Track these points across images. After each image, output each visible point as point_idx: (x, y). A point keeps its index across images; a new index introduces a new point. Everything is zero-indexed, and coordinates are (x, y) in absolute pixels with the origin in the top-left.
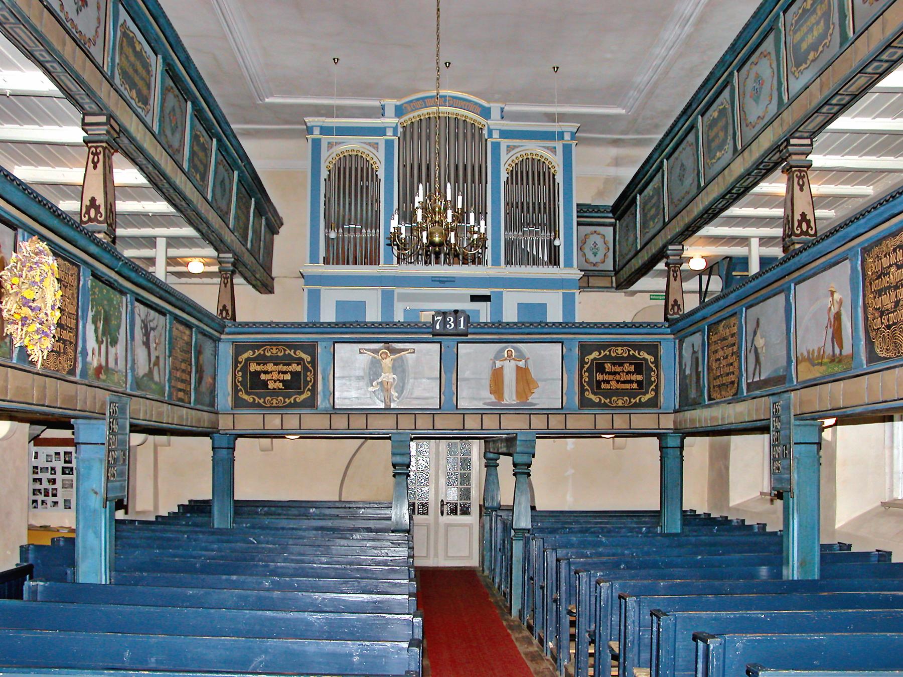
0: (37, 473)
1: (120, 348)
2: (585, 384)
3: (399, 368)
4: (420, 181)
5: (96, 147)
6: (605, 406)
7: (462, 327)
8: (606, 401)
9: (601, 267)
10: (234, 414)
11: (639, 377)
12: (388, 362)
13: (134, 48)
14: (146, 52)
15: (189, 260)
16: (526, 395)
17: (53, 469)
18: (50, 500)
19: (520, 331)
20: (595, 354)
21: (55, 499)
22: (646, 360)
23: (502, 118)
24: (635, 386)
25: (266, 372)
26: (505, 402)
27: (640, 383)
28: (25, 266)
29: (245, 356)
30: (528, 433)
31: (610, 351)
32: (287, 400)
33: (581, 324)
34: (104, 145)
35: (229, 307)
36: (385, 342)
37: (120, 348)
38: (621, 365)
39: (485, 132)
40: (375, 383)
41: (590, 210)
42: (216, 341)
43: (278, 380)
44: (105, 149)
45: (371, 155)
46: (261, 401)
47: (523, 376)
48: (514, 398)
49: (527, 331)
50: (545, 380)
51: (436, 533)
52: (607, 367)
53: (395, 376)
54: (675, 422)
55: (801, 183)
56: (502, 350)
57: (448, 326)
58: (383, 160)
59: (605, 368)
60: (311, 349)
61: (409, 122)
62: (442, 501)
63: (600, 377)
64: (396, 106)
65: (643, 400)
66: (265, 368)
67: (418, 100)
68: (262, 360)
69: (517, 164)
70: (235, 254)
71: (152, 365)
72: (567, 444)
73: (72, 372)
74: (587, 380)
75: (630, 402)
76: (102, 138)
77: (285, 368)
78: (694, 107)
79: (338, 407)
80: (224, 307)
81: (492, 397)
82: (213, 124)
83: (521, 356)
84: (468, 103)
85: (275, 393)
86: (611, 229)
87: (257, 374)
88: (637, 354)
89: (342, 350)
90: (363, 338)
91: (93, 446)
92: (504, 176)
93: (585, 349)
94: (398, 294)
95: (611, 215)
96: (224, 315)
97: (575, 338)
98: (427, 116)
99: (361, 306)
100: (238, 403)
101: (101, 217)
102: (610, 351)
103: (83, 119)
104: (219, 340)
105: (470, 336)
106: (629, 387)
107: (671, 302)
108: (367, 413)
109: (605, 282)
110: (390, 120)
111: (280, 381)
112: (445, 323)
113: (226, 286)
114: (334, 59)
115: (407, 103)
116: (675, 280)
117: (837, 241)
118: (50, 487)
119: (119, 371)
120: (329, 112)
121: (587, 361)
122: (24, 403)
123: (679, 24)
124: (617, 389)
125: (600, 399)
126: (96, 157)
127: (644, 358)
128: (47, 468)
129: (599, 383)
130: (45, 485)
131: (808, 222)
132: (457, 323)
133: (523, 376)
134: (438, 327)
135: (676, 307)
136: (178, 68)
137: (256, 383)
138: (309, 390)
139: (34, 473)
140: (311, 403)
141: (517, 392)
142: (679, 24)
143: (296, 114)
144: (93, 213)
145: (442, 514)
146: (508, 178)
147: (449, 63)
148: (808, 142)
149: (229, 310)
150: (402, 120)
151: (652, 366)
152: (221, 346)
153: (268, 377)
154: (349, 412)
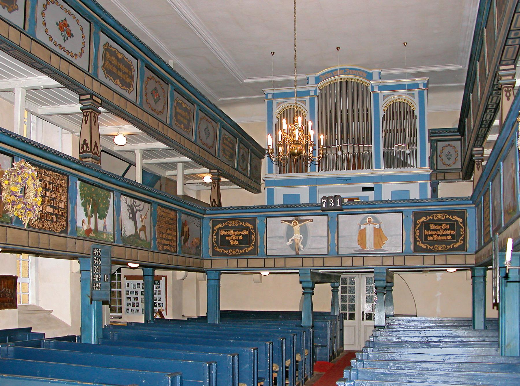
0: (129, 294)
1: (109, 220)
2: (417, 237)
3: (304, 231)
4: (284, 118)
5: (87, 112)
6: (430, 251)
7: (338, 205)
8: (431, 248)
9: (453, 167)
10: (211, 259)
11: (452, 232)
12: (297, 228)
13: (117, 57)
14: (127, 59)
15: (204, 175)
16: (380, 245)
17: (136, 292)
18: (135, 308)
19: (375, 206)
20: (423, 219)
21: (137, 308)
22: (457, 221)
23: (380, 78)
24: (450, 237)
25: (229, 236)
26: (367, 249)
27: (452, 236)
28: (12, 175)
29: (218, 226)
30: (382, 267)
31: (433, 216)
32: (241, 251)
33: (413, 200)
34: (91, 110)
35: (216, 200)
36: (295, 216)
37: (109, 220)
38: (441, 225)
39: (370, 88)
40: (290, 240)
41: (445, 131)
42: (202, 219)
43: (236, 240)
44: (91, 113)
45: (302, 108)
46: (227, 252)
47: (378, 233)
48: (373, 247)
49: (379, 206)
50: (392, 236)
51: (359, 331)
52: (431, 226)
53: (301, 236)
54: (476, 260)
55: (508, 95)
56: (365, 218)
57: (330, 205)
58: (308, 110)
59: (430, 227)
60: (253, 221)
61: (324, 86)
62: (363, 312)
63: (427, 233)
64: (315, 78)
65: (455, 246)
66: (229, 233)
67: (328, 72)
68: (227, 229)
69: (390, 106)
70: (218, 170)
71: (138, 230)
72: (436, 277)
73: (65, 231)
74: (418, 235)
75: (447, 248)
77: (239, 233)
78: (474, 55)
80: (214, 200)
81: (359, 246)
82: (190, 96)
83: (377, 221)
84: (358, 72)
85: (234, 247)
86: (459, 142)
87: (225, 236)
88: (451, 218)
89: (271, 221)
90: (282, 214)
91: (86, 272)
92: (382, 114)
93: (417, 215)
94: (319, 189)
95: (458, 134)
97: (410, 209)
98: (334, 82)
99: (298, 196)
100: (215, 253)
101: (89, 149)
102: (433, 216)
103: (80, 98)
104: (203, 218)
105: (344, 211)
106: (445, 239)
108: (285, 257)
109: (456, 176)
110: (312, 86)
111: (237, 240)
112: (328, 203)
113: (214, 188)
114: (272, 53)
115: (321, 75)
117: (507, 129)
118: (135, 302)
119: (108, 233)
120: (277, 84)
121: (418, 223)
122: (20, 246)
123: (472, 4)
124: (438, 240)
125: (245, 225)
126: (87, 117)
127: (456, 220)
128: (134, 292)
129: (426, 236)
130: (133, 300)
132: (335, 203)
133: (378, 233)
134: (324, 206)
135: (85, 146)
136: (153, 65)
137: (223, 242)
138: (253, 245)
139: (127, 294)
140: (254, 253)
141: (374, 243)
142: (472, 4)
143: (258, 88)
145: (363, 320)
146: (384, 115)
147: (339, 48)
148: (512, 67)
149: (216, 204)
150: (319, 85)
151: (461, 225)
152: (205, 221)
153: (231, 238)
154: (275, 257)
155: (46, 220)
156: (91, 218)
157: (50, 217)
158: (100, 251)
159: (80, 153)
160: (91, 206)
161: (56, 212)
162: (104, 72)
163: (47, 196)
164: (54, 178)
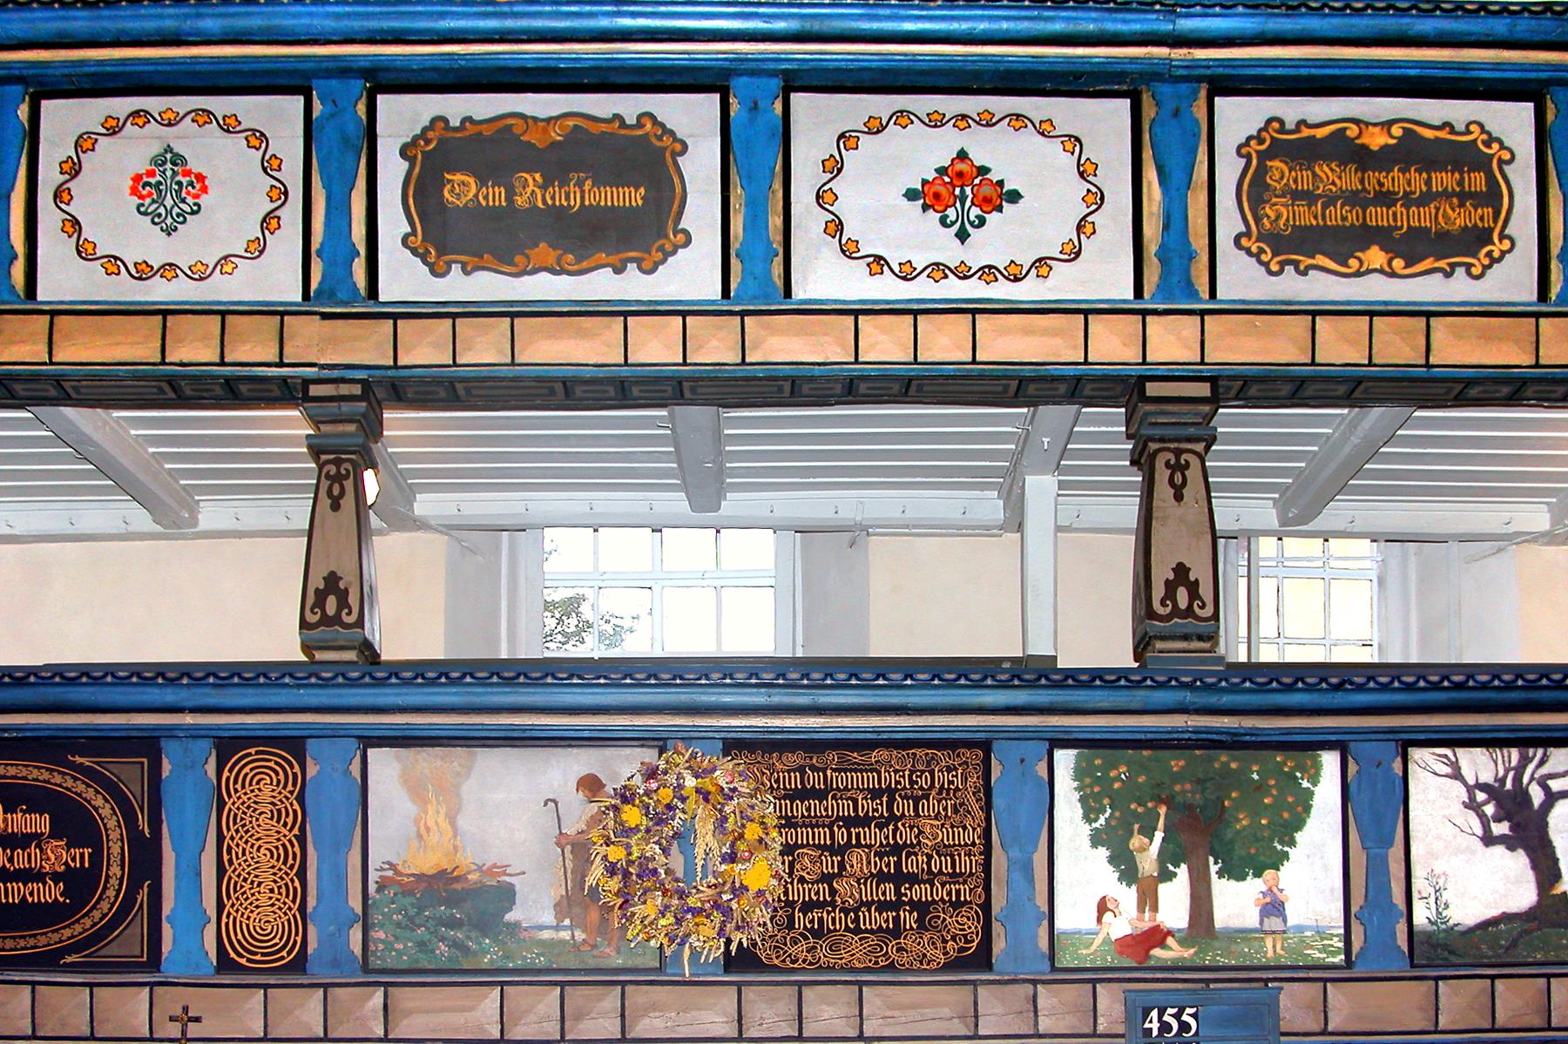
55: (336, 492)
76: (349, 441)
79: (1065, 964)
96: (1183, 602)
101: (349, 614)
107: (1162, 573)
116: (1179, 497)
131: (343, 597)
144: (331, 605)
155: (857, 931)
156: (1163, 888)
157: (875, 919)
158: (1194, 1016)
159: (304, 624)
160: (1159, 836)
161: (919, 892)
162: (1257, 256)
163: (859, 845)
164: (896, 771)
